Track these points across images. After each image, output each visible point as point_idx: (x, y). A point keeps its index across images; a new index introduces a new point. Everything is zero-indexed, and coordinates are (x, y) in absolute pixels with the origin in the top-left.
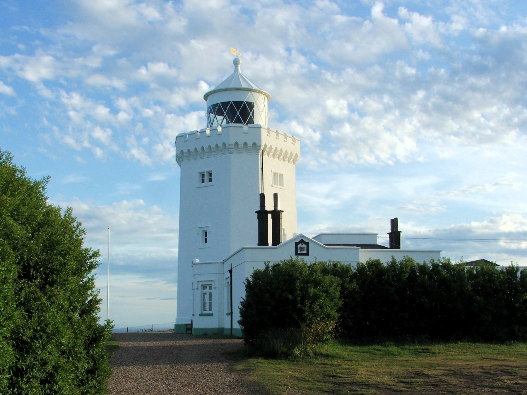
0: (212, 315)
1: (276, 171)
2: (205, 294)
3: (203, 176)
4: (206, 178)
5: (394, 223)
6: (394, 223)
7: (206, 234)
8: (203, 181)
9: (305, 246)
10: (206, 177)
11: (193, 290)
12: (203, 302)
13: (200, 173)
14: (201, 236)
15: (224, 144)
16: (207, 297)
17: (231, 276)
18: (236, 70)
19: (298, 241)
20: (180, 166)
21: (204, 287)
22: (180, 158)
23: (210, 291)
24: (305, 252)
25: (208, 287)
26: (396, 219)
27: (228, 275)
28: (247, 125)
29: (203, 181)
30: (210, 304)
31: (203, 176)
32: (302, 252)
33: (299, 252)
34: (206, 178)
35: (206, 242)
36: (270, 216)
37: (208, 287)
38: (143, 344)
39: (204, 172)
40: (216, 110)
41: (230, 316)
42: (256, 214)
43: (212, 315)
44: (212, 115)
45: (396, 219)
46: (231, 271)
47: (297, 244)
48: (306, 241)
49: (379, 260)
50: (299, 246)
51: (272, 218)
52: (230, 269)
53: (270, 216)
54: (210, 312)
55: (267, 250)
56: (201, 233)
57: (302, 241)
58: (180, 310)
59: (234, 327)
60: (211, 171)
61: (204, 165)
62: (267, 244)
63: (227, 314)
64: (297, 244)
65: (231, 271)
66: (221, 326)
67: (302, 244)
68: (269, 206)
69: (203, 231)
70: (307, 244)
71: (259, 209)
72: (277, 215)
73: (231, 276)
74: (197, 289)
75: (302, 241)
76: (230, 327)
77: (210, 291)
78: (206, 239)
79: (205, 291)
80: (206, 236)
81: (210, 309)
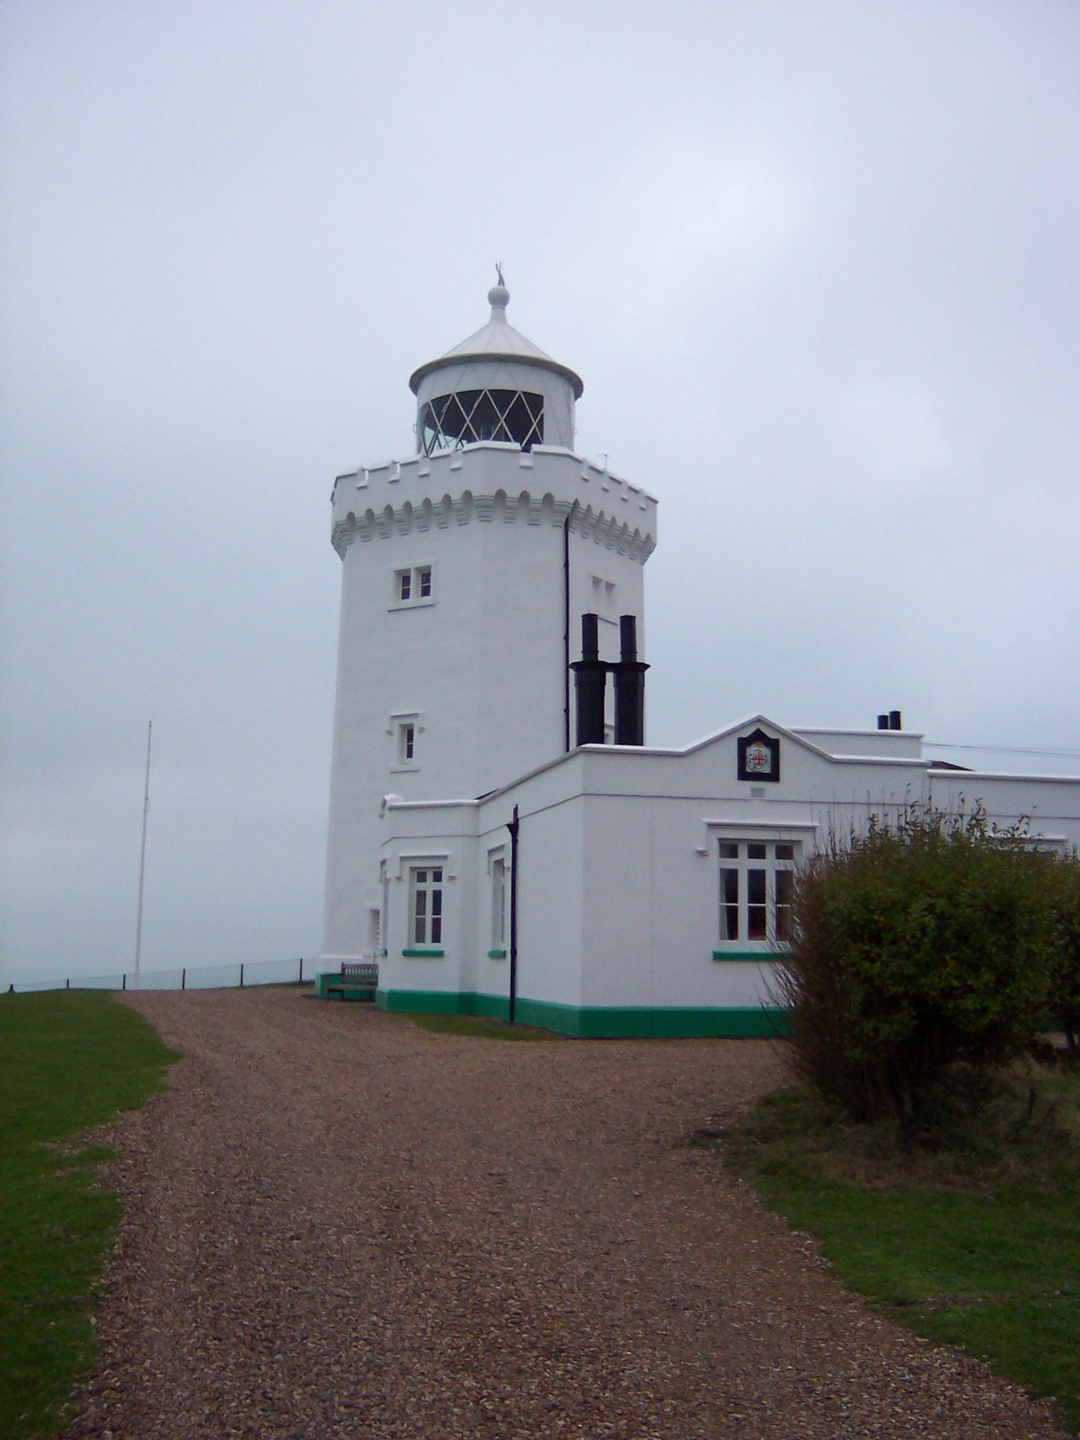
0: (440, 954)
1: (600, 575)
3: (406, 580)
4: (415, 586)
6: (516, 809)
8: (406, 595)
9: (765, 751)
11: (386, 882)
12: (429, 916)
13: (398, 573)
14: (396, 741)
15: (468, 495)
17: (515, 842)
19: (746, 734)
20: (342, 556)
21: (422, 877)
22: (347, 532)
24: (766, 769)
25: (430, 877)
27: (506, 838)
29: (406, 595)
30: (437, 924)
31: (406, 580)
32: (759, 769)
33: (748, 770)
34: (415, 586)
35: (410, 755)
36: (610, 677)
37: (430, 877)
39: (409, 570)
40: (444, 410)
43: (440, 954)
44: (429, 433)
46: (514, 828)
47: (743, 744)
48: (771, 735)
50: (752, 751)
51: (618, 685)
52: (510, 820)
53: (610, 677)
55: (637, 760)
56: (397, 731)
57: (758, 737)
59: (142, 969)
60: (429, 568)
61: (411, 551)
63: (497, 955)
64: (743, 744)
65: (514, 828)
66: (467, 990)
68: (609, 651)
69: (403, 727)
70: (774, 745)
72: (631, 673)
73: (515, 842)
74: (399, 879)
75: (758, 737)
76: (507, 994)
79: (421, 886)
80: (410, 738)
81: (436, 938)
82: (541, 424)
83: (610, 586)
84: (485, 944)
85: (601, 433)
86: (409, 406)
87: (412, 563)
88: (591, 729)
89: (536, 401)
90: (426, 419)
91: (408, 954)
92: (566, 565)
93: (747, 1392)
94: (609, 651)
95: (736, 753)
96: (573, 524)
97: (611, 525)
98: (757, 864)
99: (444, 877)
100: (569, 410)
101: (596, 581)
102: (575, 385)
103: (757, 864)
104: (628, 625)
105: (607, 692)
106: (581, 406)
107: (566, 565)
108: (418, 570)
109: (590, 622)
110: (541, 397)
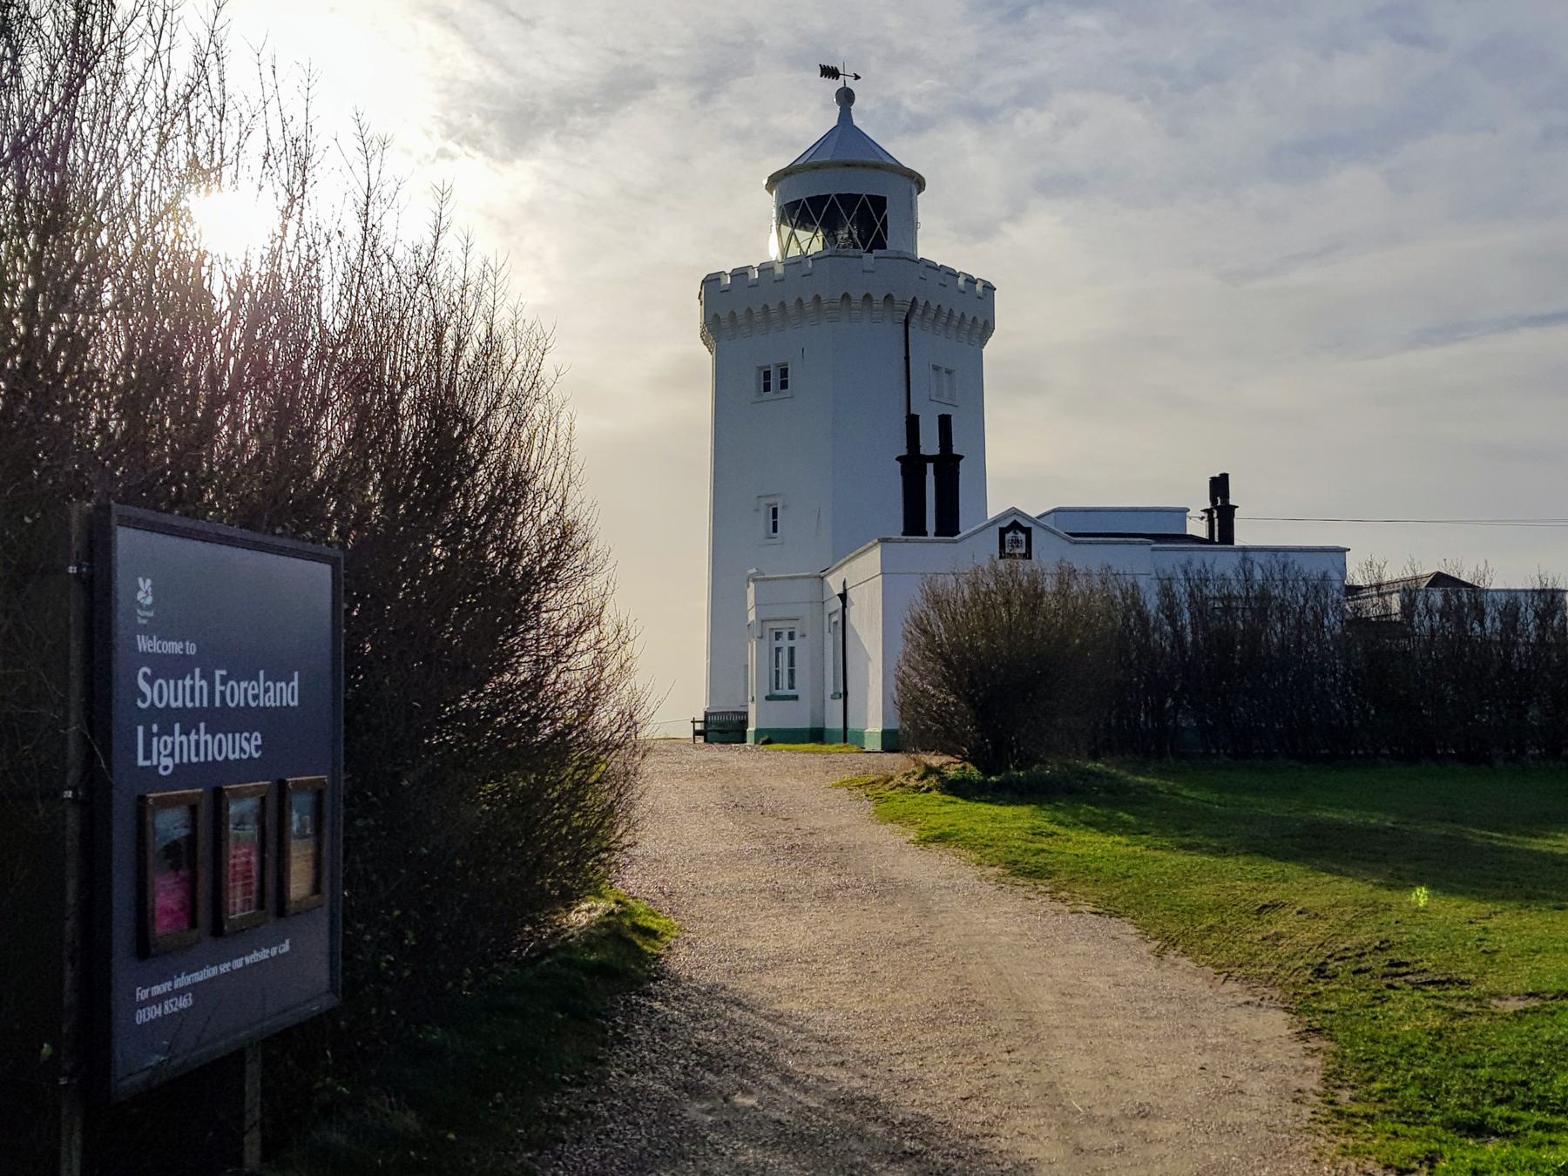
0: (796, 698)
2: (778, 650)
3: (767, 375)
4: (775, 380)
5: (1220, 486)
6: (1220, 486)
7: (775, 511)
8: (767, 388)
9: (1022, 537)
10: (775, 379)
13: (760, 368)
14: (763, 521)
16: (784, 657)
17: (844, 606)
18: (845, 116)
19: (1005, 524)
23: (792, 644)
26: (1225, 477)
28: (870, 251)
29: (767, 388)
31: (767, 375)
33: (1023, 551)
34: (775, 380)
35: (775, 530)
36: (930, 467)
37: (785, 635)
38: (165, 987)
41: (841, 701)
42: (899, 464)
45: (1225, 477)
47: (1003, 532)
48: (1025, 524)
49: (711, 283)
50: (1009, 536)
53: (930, 467)
54: (791, 692)
57: (1015, 526)
58: (713, 692)
62: (925, 534)
64: (1003, 532)
65: (843, 597)
67: (1015, 532)
68: (930, 445)
70: (1028, 531)
71: (904, 452)
72: (948, 464)
73: (844, 606)
75: (1015, 526)
76: (841, 726)
77: (792, 644)
78: (775, 524)
81: (791, 687)
84: (830, 691)
86: (768, 204)
87: (772, 361)
89: (880, 203)
90: (782, 220)
91: (767, 698)
92: (907, 358)
93: (103, 312)
94: (930, 445)
95: (703, 604)
96: (913, 321)
99: (797, 636)
101: (936, 368)
102: (920, 183)
104: (945, 422)
105: (933, 482)
106: (922, 199)
107: (907, 358)
109: (912, 423)
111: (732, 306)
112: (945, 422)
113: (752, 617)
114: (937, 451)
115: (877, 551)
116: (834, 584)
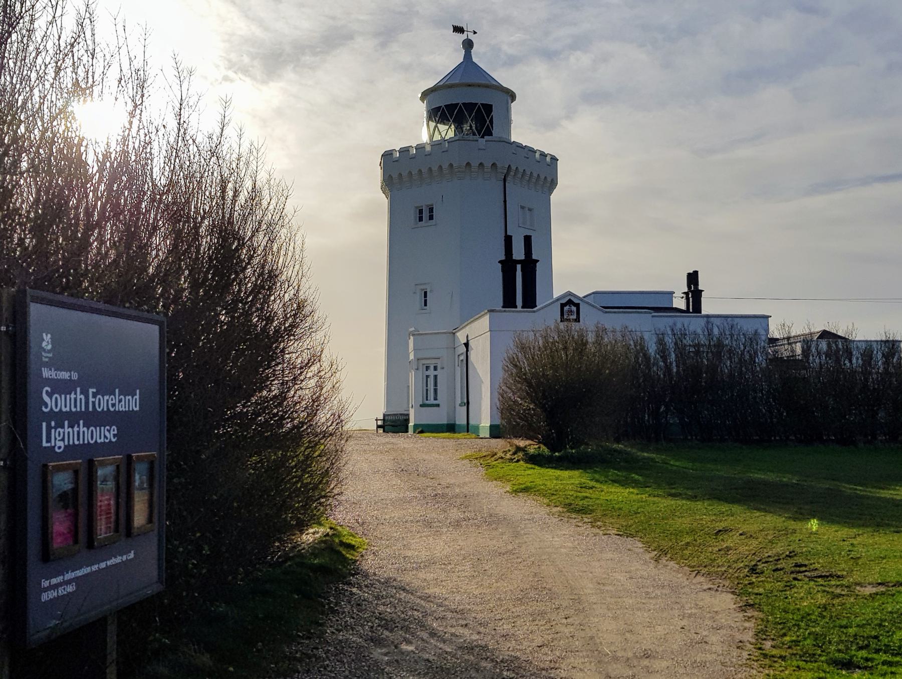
0: (438, 405)
3: (421, 212)
4: (426, 215)
7: (426, 293)
8: (421, 219)
9: (574, 309)
10: (426, 214)
14: (419, 298)
17: (467, 351)
19: (564, 301)
29: (421, 219)
30: (436, 391)
31: (421, 212)
34: (426, 215)
35: (426, 305)
36: (519, 267)
48: (576, 301)
50: (566, 308)
52: (465, 341)
53: (519, 267)
57: (570, 302)
59: (471, 422)
64: (563, 306)
65: (467, 345)
68: (519, 253)
70: (577, 306)
72: (530, 265)
73: (467, 351)
75: (570, 302)
78: (426, 301)
79: (428, 373)
80: (425, 296)
81: (435, 399)
82: (491, 122)
83: (530, 210)
84: (458, 401)
85: (523, 130)
86: (422, 109)
87: (424, 203)
88: (509, 302)
89: (488, 108)
91: (421, 406)
92: (505, 201)
93: (22, 173)
94: (519, 253)
96: (509, 179)
97: (540, 172)
98: (436, 373)
99: (439, 368)
100: (508, 111)
101: (523, 207)
102: (512, 96)
103: (436, 373)
104: (528, 240)
105: (520, 276)
108: (427, 206)
109: (508, 240)
110: (491, 106)
111: (401, 171)
112: (528, 240)
113: (412, 357)
114: (522, 257)
115: (487, 317)
116: (461, 337)
